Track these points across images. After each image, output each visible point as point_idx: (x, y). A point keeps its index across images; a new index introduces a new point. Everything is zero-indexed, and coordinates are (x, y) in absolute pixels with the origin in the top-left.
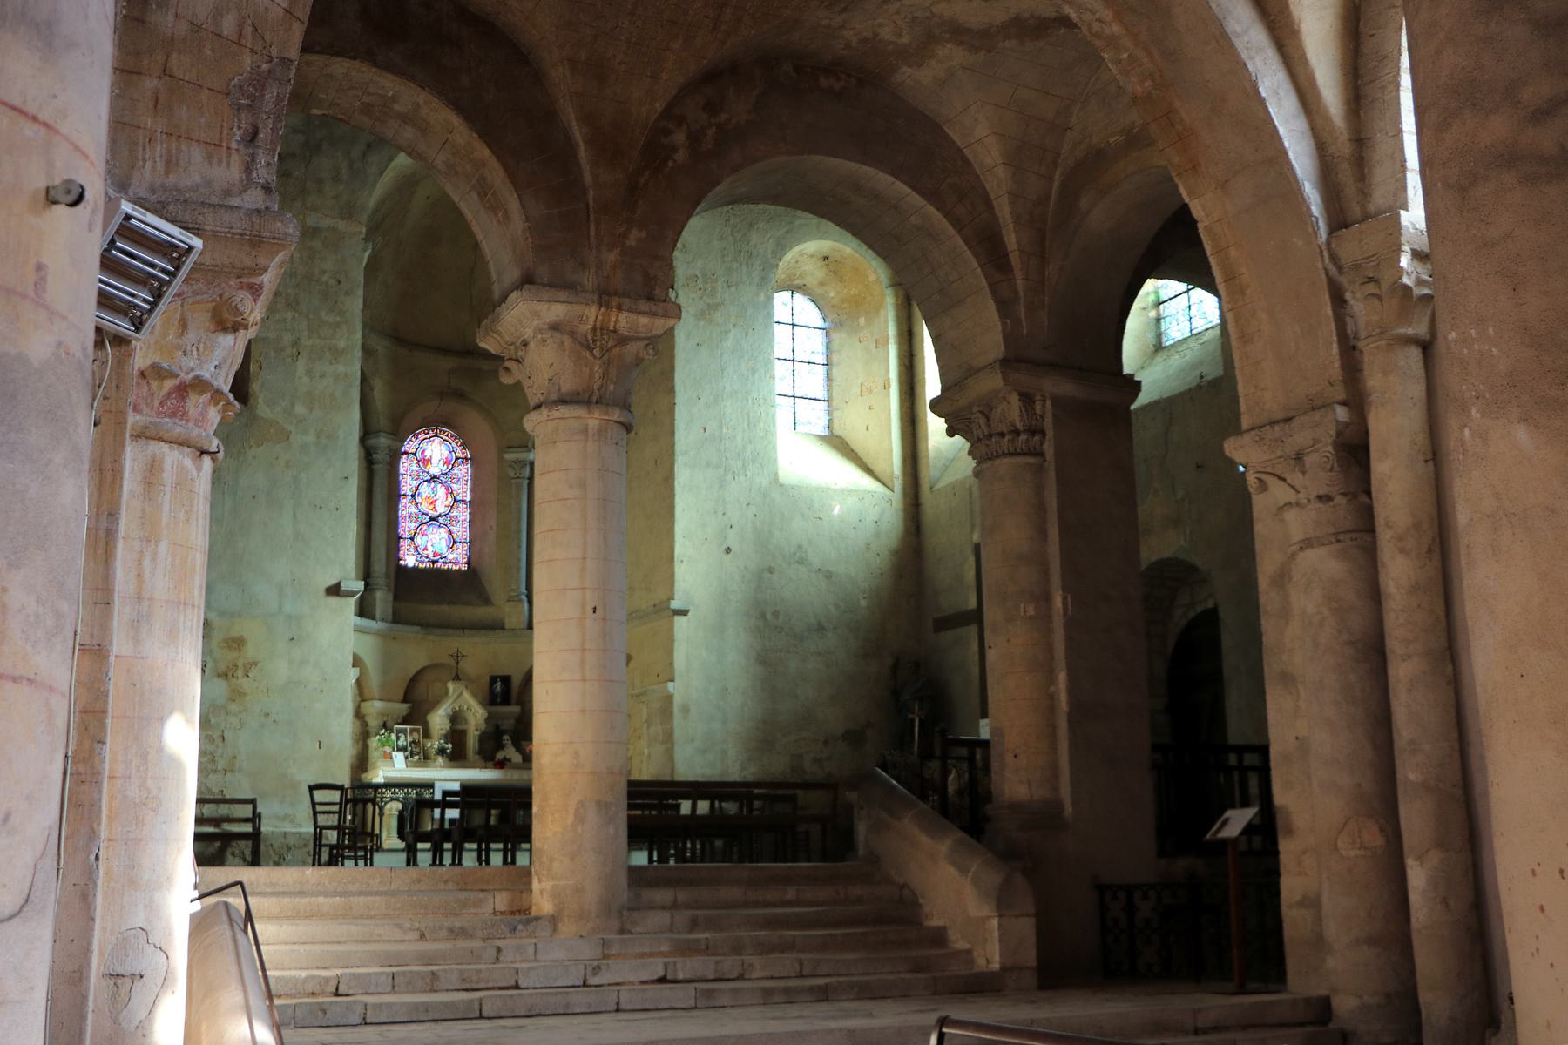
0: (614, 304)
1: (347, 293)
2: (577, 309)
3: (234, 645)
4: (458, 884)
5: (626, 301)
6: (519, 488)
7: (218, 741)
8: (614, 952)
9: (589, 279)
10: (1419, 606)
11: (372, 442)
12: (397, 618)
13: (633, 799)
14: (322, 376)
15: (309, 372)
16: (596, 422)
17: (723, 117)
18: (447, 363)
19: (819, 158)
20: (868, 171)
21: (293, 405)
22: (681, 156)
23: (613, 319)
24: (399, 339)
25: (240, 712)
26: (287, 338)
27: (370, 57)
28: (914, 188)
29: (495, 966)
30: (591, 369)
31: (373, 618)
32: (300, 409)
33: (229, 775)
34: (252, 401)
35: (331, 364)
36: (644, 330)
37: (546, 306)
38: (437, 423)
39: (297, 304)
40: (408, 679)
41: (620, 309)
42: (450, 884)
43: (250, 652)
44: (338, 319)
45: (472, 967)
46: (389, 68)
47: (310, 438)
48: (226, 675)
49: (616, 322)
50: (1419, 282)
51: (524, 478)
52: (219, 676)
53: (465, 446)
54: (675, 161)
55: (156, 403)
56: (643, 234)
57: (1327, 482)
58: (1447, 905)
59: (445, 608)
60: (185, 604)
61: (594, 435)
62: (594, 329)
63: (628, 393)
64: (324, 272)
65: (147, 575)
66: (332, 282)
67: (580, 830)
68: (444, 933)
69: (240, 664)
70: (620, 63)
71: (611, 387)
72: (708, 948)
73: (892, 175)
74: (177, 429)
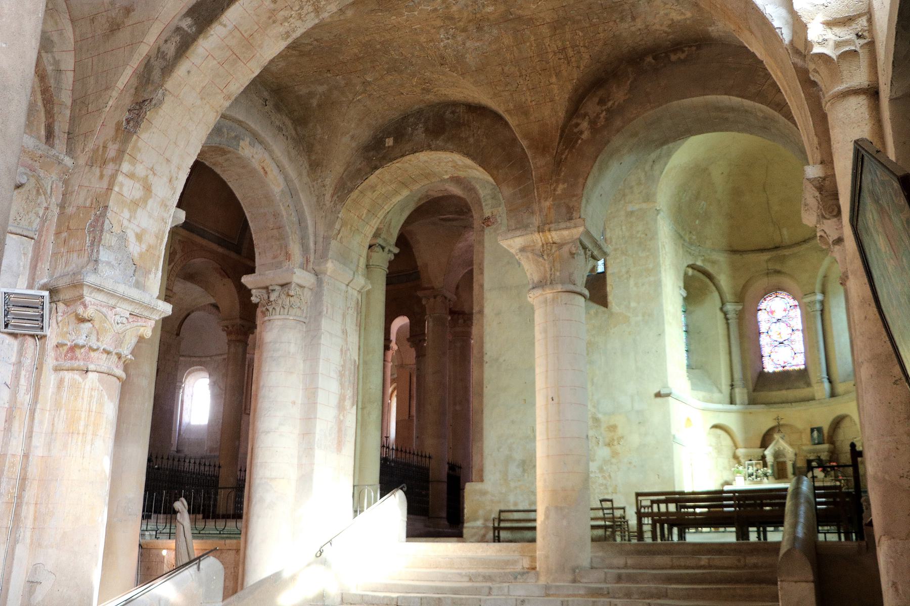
0: (546, 229)
1: (651, 239)
2: (529, 238)
3: (612, 429)
4: (520, 552)
5: (553, 226)
6: (815, 317)
7: (608, 478)
8: (552, 593)
9: (536, 220)
10: (866, 317)
11: (725, 309)
12: (752, 401)
13: (782, 503)
14: (643, 285)
15: (636, 284)
16: (551, 295)
17: (610, 104)
18: (766, 256)
19: (675, 103)
20: (711, 98)
21: (629, 303)
22: (585, 135)
23: (550, 237)
24: (733, 251)
25: (617, 463)
26: (624, 270)
27: (429, 148)
28: (742, 97)
29: (488, 597)
30: (544, 267)
31: (735, 404)
32: (633, 304)
33: (614, 494)
34: (609, 306)
35: (646, 277)
36: (568, 238)
37: (512, 241)
38: (776, 289)
39: (627, 252)
40: (762, 435)
41: (549, 230)
42: (516, 552)
43: (620, 431)
44: (648, 253)
45: (477, 597)
46: (437, 149)
47: (640, 318)
48: (609, 445)
49: (552, 238)
50: (837, 44)
51: (816, 311)
52: (606, 445)
53: (794, 298)
54: (582, 139)
55: (63, 356)
56: (566, 185)
57: (836, 227)
58: (897, 590)
59: (784, 392)
60: (72, 433)
61: (550, 302)
62: (543, 245)
63: (571, 275)
64: (638, 232)
65: (56, 424)
66: (643, 236)
67: (547, 523)
68: (481, 579)
69: (615, 438)
70: (531, 102)
71: (558, 274)
72: (608, 593)
73: (726, 94)
74: (75, 364)
